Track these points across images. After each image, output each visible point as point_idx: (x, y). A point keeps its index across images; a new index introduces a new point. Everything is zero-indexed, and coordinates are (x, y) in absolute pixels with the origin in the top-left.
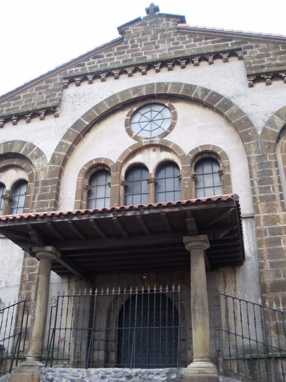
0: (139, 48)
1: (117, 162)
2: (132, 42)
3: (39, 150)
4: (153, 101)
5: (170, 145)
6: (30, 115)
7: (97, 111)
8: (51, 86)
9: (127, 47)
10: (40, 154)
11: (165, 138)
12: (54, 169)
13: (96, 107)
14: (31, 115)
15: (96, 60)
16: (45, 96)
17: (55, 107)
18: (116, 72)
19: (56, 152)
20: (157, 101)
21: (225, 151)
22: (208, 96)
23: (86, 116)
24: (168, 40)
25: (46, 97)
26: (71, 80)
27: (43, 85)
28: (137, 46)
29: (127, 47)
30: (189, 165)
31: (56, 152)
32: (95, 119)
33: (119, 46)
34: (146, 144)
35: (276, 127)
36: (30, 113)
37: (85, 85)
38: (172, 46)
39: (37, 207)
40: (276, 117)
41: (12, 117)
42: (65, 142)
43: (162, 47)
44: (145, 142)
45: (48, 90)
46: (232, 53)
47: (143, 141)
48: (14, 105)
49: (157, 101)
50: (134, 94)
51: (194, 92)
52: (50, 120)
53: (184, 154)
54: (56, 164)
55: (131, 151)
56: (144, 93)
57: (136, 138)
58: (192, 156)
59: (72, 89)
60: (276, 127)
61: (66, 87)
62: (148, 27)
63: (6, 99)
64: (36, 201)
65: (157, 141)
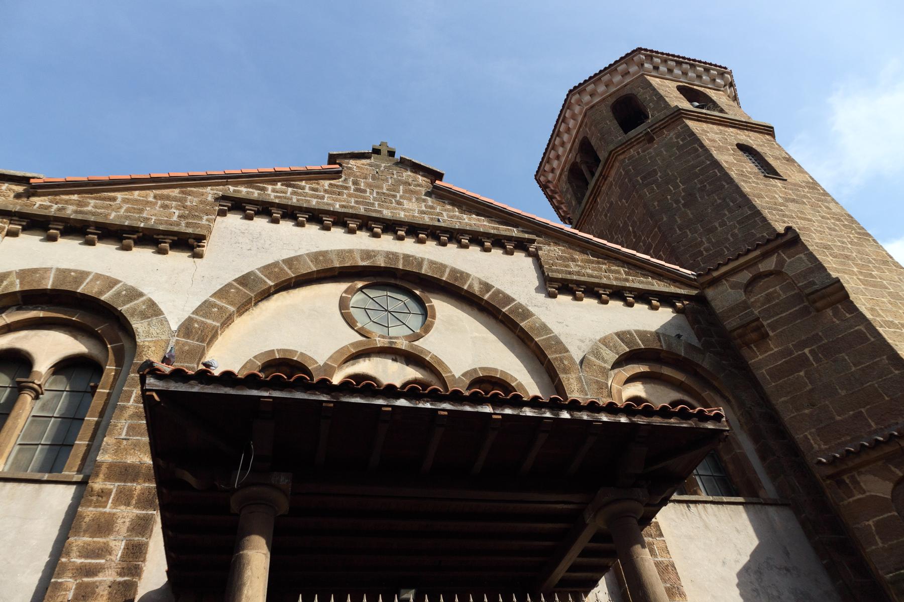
0: (368, 194)
1: (325, 364)
2: (355, 183)
3: (152, 304)
4: (393, 281)
5: (427, 355)
6: (135, 236)
7: (290, 269)
8: (192, 201)
9: (347, 188)
10: (153, 310)
11: (416, 343)
12: (187, 348)
13: (289, 262)
14: (138, 237)
15: (290, 190)
16: (177, 214)
17: (200, 238)
18: (328, 220)
19: (194, 316)
20: (398, 282)
21: (523, 383)
22: (490, 293)
23: (268, 269)
24: (417, 199)
25: (179, 217)
26: (238, 205)
27: (173, 194)
28: (364, 191)
29: (347, 188)
30: (840, 307)
31: (194, 316)
32: (283, 282)
33: (332, 182)
34: (382, 345)
35: (605, 362)
36: (138, 232)
37: (260, 223)
38: (424, 208)
39: (131, 417)
40: (602, 346)
41: (88, 227)
42: (218, 302)
43: (406, 204)
44: (380, 342)
45: (185, 207)
46: (521, 245)
47: (377, 339)
48: (95, 207)
49: (398, 282)
50: (362, 259)
51: (468, 283)
52: (178, 259)
53: (453, 375)
54: (193, 339)
55: (353, 351)
56: (381, 262)
57: (360, 332)
58: (467, 382)
59: (234, 220)
60: (605, 362)
61: (222, 213)
62: (382, 172)
63: (79, 193)
64: (131, 403)
65: (402, 344)
